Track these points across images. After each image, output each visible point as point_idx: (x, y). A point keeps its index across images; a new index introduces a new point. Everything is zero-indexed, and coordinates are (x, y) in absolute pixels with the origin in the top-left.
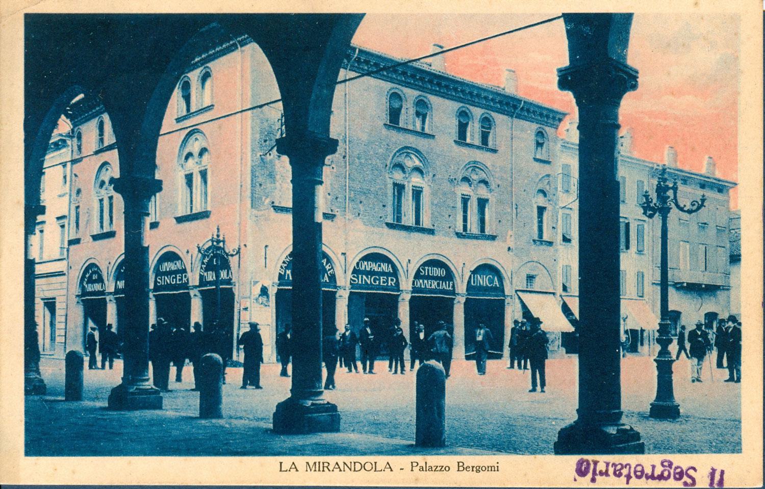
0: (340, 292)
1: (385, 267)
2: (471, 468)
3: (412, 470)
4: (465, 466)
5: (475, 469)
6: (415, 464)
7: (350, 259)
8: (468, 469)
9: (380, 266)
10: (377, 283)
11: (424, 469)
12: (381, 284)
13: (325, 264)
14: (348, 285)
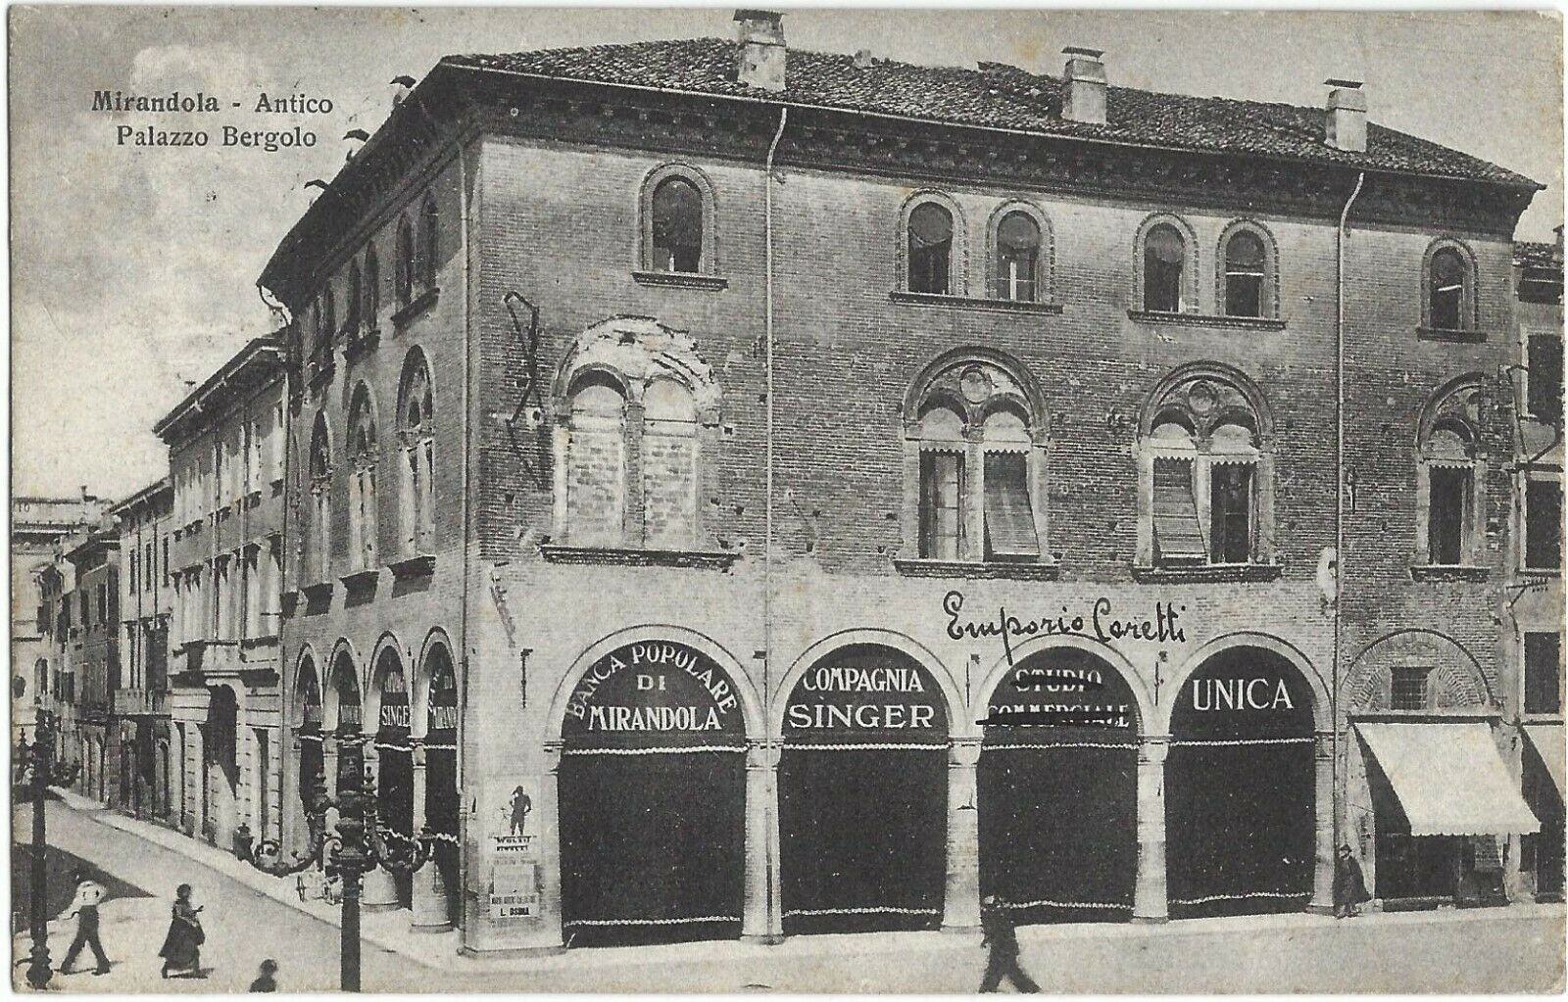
0: (756, 754)
1: (897, 679)
2: (253, 137)
3: (121, 142)
4: (238, 135)
5: (262, 140)
6: (125, 131)
7: (778, 667)
8: (246, 140)
9: (881, 677)
10: (875, 723)
11: (147, 141)
12: (888, 725)
13: (707, 685)
14: (777, 733)
